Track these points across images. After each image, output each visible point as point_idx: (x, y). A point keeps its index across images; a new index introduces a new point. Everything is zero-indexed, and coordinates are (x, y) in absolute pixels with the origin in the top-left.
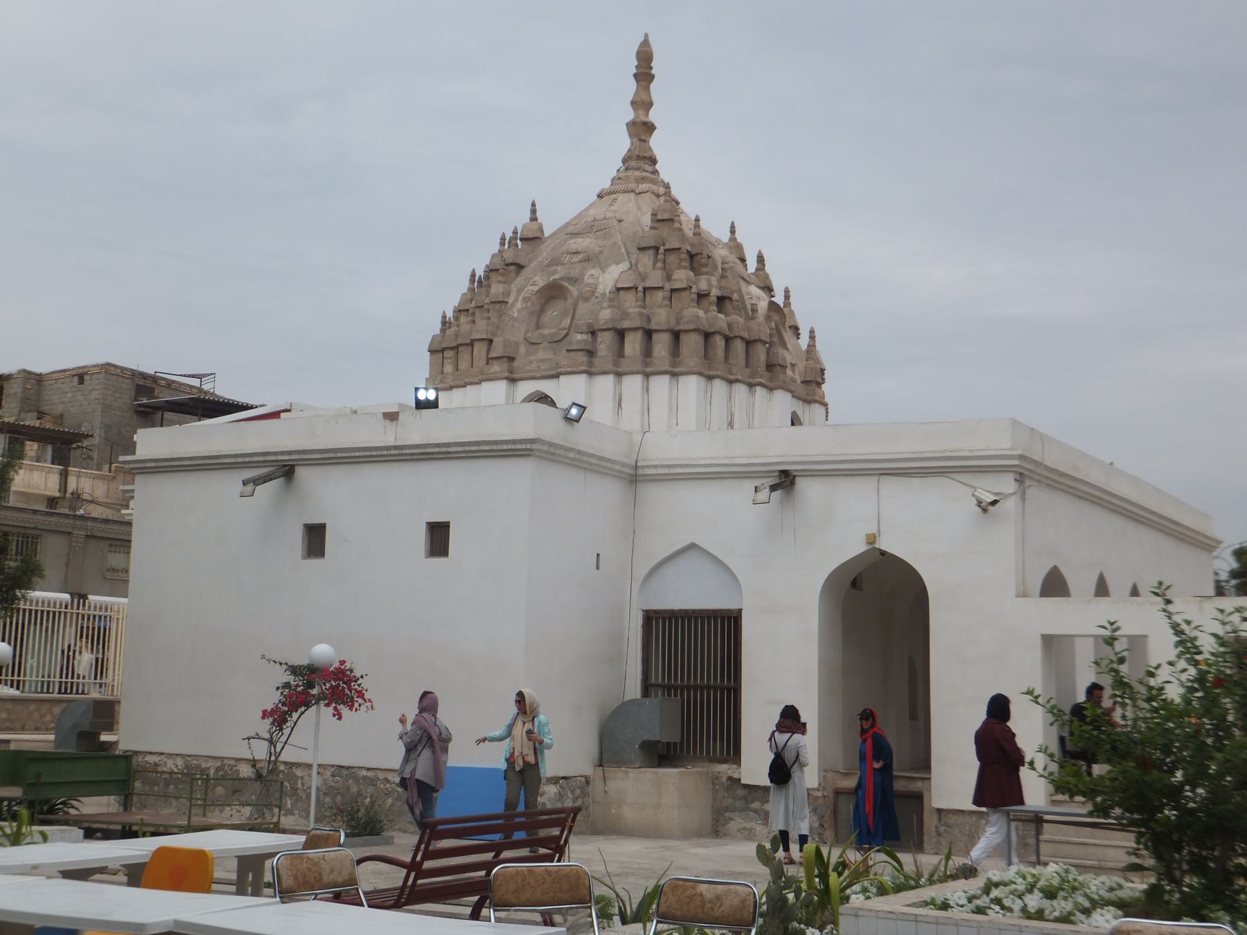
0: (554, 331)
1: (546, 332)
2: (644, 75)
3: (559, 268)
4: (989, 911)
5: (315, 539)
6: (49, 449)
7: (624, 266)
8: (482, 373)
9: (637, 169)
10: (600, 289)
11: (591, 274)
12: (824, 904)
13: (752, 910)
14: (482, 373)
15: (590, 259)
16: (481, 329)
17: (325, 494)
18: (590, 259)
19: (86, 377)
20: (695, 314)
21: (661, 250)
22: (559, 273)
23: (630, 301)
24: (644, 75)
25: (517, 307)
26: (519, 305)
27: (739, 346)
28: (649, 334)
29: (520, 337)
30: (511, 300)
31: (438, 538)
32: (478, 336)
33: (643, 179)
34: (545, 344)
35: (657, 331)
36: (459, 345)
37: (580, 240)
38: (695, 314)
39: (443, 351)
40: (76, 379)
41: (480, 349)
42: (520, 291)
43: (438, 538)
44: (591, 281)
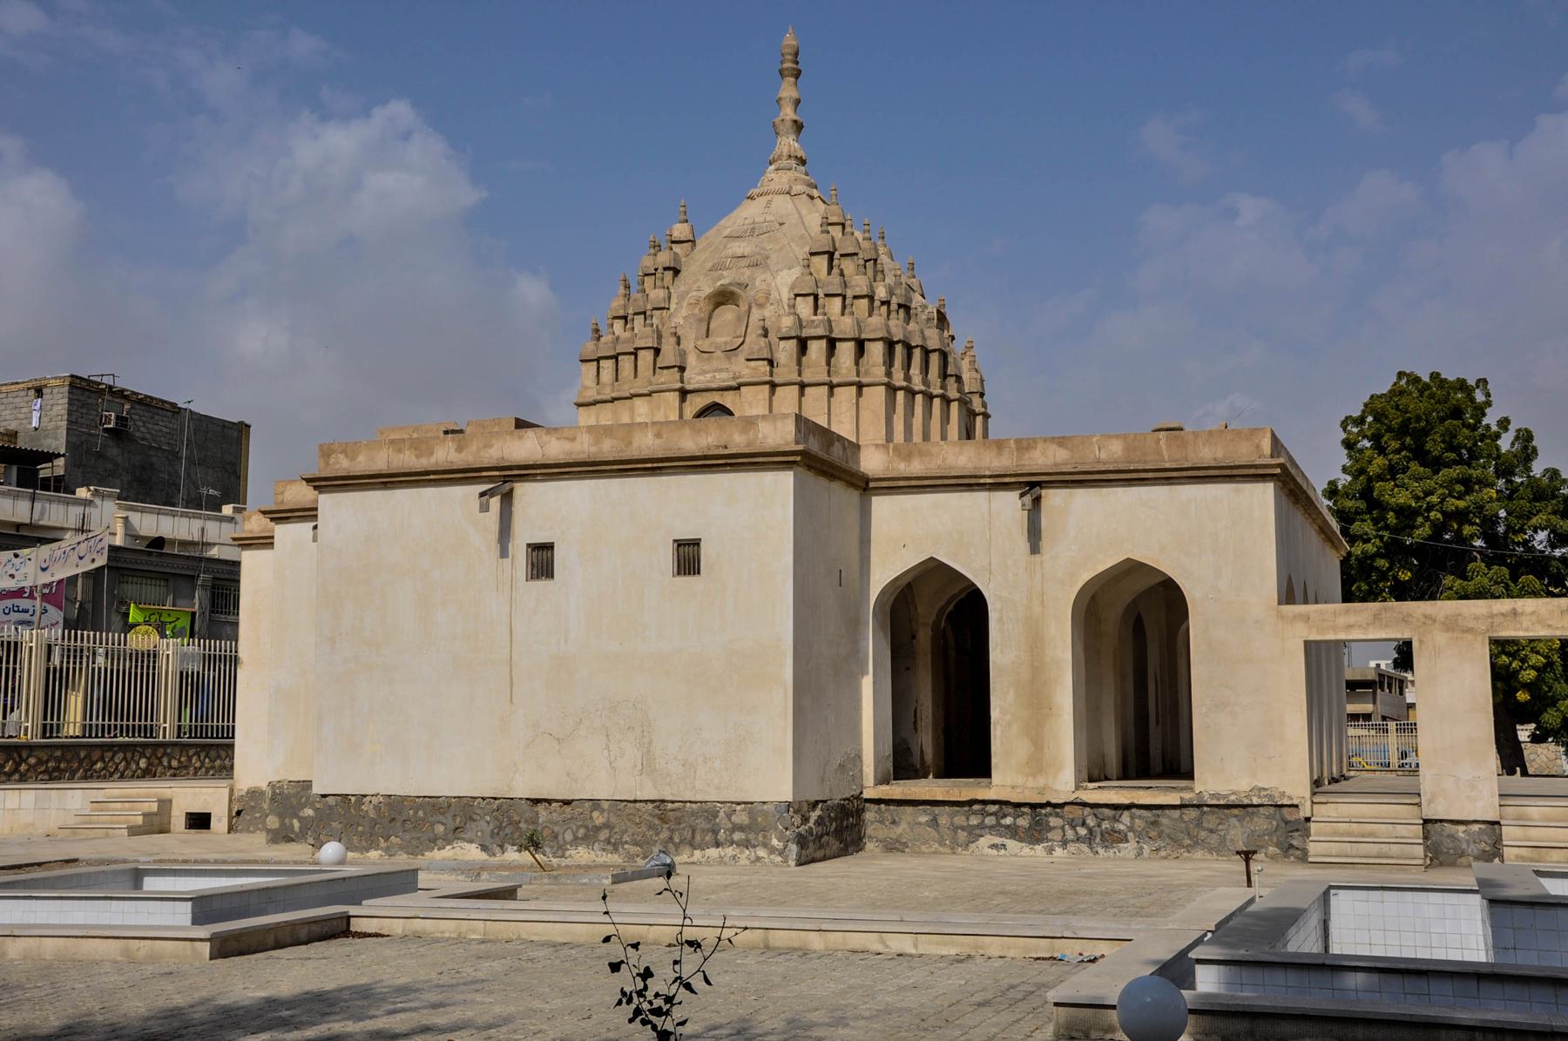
1: (720, 340)
4: (369, 914)
5: (542, 560)
6: (14, 469)
7: (796, 272)
8: (650, 383)
11: (760, 279)
13: (1375, 977)
14: (650, 383)
15: (759, 263)
17: (543, 508)
18: (759, 263)
19: (45, 391)
20: (875, 324)
21: (837, 255)
22: (726, 278)
23: (805, 307)
28: (832, 343)
31: (688, 557)
34: (719, 353)
35: (841, 340)
38: (875, 324)
40: (32, 392)
41: (646, 357)
42: (681, 298)
43: (688, 557)
44: (764, 287)
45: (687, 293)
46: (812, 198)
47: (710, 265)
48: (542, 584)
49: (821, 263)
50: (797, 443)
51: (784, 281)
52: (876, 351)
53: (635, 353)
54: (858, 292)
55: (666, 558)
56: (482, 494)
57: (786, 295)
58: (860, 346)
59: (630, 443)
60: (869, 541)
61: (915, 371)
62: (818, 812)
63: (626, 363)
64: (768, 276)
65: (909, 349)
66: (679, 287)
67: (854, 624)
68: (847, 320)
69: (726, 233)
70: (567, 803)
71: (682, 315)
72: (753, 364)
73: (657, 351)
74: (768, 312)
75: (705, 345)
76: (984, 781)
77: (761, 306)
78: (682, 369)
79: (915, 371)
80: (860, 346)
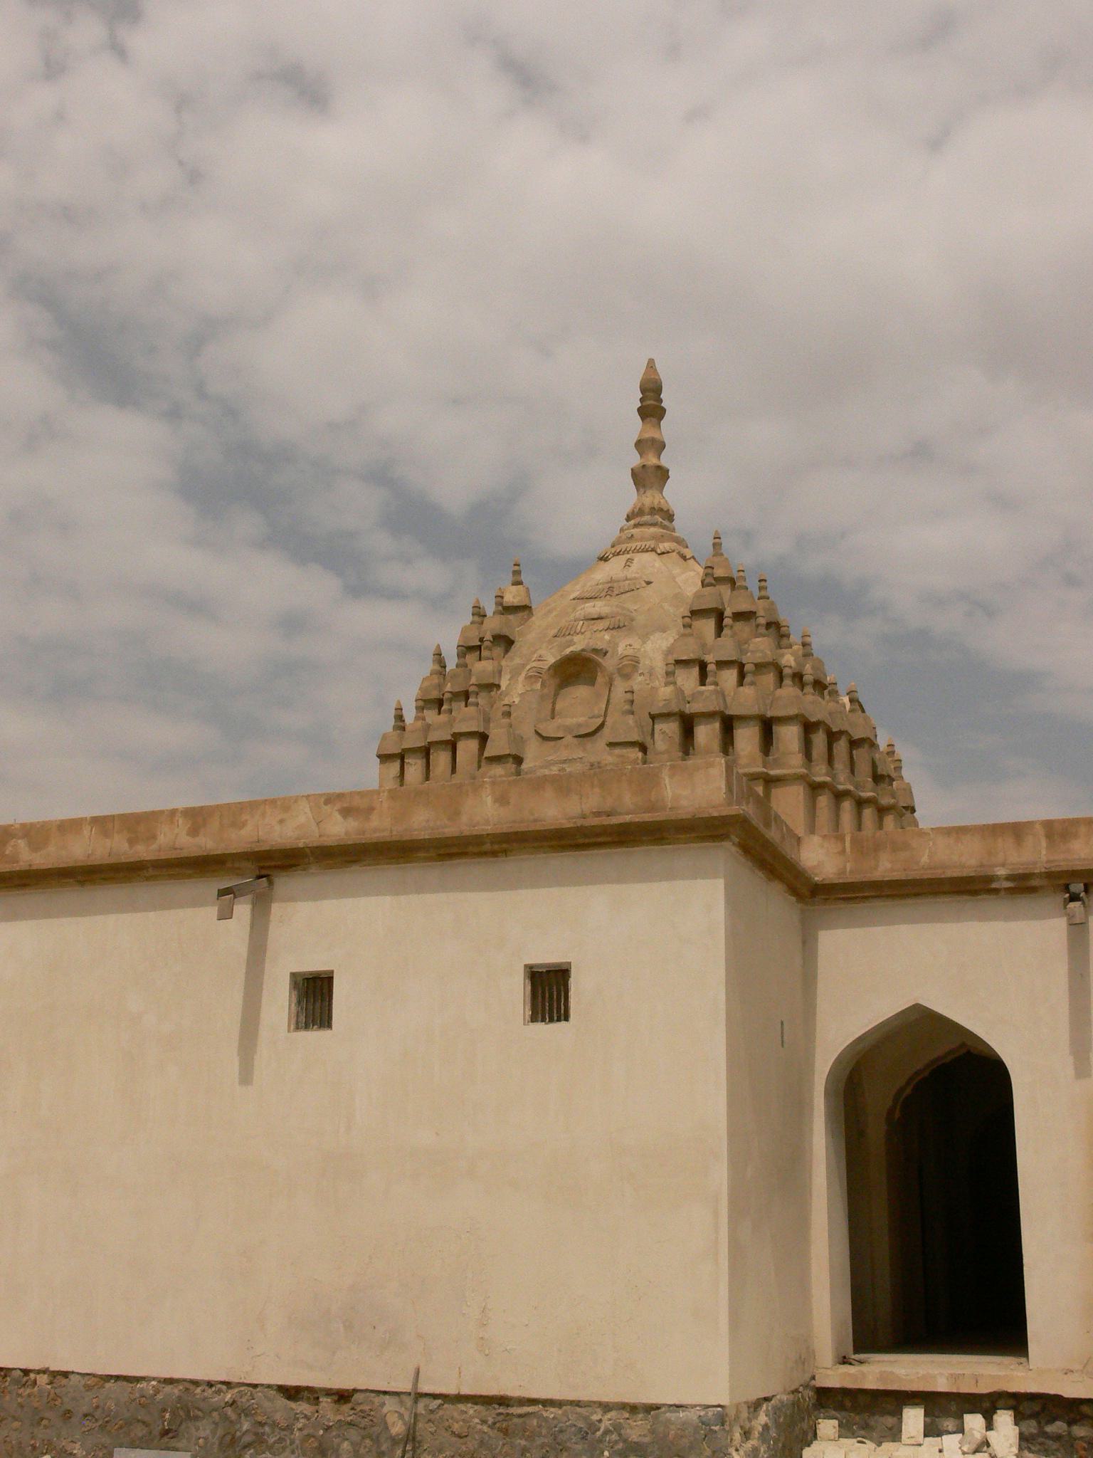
0: (581, 720)
1: (570, 721)
2: (651, 409)
3: (576, 638)
5: (314, 996)
9: (654, 525)
10: (645, 663)
12: (111, 1454)
16: (465, 718)
22: (579, 644)
23: (687, 680)
24: (651, 409)
25: (515, 689)
26: (520, 687)
27: (841, 746)
29: (527, 730)
30: (504, 684)
31: (549, 991)
32: (464, 729)
33: (661, 538)
34: (569, 739)
36: (458, 736)
37: (599, 603)
38: (788, 700)
39: (401, 757)
41: (467, 749)
43: (549, 991)
45: (524, 666)
46: (684, 558)
47: (554, 631)
48: (315, 1037)
49: (708, 625)
50: (730, 804)
51: (655, 649)
52: (789, 736)
53: (452, 745)
54: (758, 658)
55: (517, 990)
56: (222, 893)
57: (660, 666)
58: (767, 727)
59: (457, 813)
60: (815, 977)
61: (840, 766)
62: (762, 1418)
63: (441, 759)
64: (635, 641)
65: (832, 737)
66: (515, 658)
67: (800, 1107)
68: (747, 691)
69: (575, 594)
70: (343, 1397)
71: (516, 688)
72: (617, 751)
73: (483, 738)
74: (638, 682)
75: (549, 729)
76: (1023, 1360)
77: (627, 677)
78: (518, 760)
79: (840, 766)
80: (767, 727)
